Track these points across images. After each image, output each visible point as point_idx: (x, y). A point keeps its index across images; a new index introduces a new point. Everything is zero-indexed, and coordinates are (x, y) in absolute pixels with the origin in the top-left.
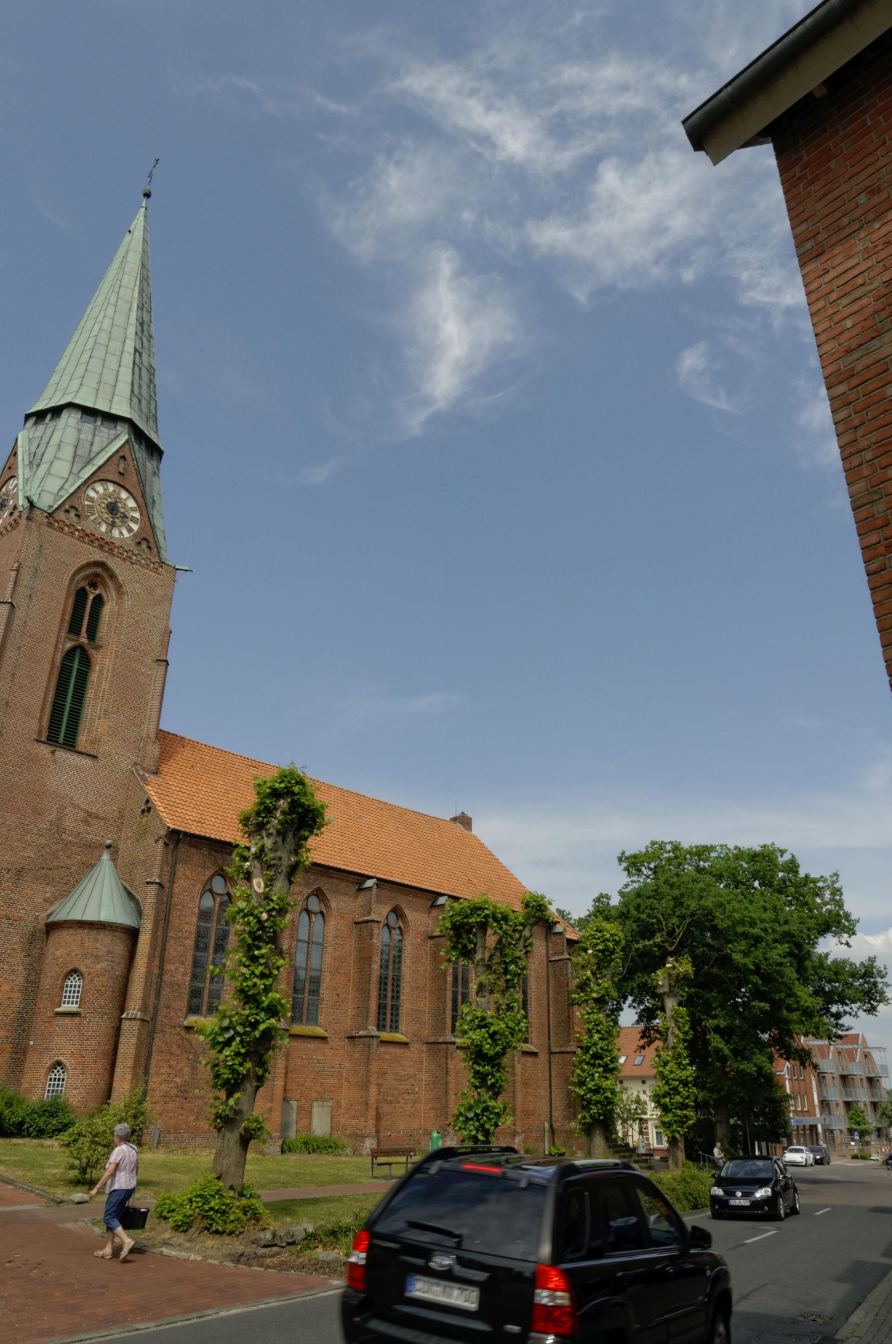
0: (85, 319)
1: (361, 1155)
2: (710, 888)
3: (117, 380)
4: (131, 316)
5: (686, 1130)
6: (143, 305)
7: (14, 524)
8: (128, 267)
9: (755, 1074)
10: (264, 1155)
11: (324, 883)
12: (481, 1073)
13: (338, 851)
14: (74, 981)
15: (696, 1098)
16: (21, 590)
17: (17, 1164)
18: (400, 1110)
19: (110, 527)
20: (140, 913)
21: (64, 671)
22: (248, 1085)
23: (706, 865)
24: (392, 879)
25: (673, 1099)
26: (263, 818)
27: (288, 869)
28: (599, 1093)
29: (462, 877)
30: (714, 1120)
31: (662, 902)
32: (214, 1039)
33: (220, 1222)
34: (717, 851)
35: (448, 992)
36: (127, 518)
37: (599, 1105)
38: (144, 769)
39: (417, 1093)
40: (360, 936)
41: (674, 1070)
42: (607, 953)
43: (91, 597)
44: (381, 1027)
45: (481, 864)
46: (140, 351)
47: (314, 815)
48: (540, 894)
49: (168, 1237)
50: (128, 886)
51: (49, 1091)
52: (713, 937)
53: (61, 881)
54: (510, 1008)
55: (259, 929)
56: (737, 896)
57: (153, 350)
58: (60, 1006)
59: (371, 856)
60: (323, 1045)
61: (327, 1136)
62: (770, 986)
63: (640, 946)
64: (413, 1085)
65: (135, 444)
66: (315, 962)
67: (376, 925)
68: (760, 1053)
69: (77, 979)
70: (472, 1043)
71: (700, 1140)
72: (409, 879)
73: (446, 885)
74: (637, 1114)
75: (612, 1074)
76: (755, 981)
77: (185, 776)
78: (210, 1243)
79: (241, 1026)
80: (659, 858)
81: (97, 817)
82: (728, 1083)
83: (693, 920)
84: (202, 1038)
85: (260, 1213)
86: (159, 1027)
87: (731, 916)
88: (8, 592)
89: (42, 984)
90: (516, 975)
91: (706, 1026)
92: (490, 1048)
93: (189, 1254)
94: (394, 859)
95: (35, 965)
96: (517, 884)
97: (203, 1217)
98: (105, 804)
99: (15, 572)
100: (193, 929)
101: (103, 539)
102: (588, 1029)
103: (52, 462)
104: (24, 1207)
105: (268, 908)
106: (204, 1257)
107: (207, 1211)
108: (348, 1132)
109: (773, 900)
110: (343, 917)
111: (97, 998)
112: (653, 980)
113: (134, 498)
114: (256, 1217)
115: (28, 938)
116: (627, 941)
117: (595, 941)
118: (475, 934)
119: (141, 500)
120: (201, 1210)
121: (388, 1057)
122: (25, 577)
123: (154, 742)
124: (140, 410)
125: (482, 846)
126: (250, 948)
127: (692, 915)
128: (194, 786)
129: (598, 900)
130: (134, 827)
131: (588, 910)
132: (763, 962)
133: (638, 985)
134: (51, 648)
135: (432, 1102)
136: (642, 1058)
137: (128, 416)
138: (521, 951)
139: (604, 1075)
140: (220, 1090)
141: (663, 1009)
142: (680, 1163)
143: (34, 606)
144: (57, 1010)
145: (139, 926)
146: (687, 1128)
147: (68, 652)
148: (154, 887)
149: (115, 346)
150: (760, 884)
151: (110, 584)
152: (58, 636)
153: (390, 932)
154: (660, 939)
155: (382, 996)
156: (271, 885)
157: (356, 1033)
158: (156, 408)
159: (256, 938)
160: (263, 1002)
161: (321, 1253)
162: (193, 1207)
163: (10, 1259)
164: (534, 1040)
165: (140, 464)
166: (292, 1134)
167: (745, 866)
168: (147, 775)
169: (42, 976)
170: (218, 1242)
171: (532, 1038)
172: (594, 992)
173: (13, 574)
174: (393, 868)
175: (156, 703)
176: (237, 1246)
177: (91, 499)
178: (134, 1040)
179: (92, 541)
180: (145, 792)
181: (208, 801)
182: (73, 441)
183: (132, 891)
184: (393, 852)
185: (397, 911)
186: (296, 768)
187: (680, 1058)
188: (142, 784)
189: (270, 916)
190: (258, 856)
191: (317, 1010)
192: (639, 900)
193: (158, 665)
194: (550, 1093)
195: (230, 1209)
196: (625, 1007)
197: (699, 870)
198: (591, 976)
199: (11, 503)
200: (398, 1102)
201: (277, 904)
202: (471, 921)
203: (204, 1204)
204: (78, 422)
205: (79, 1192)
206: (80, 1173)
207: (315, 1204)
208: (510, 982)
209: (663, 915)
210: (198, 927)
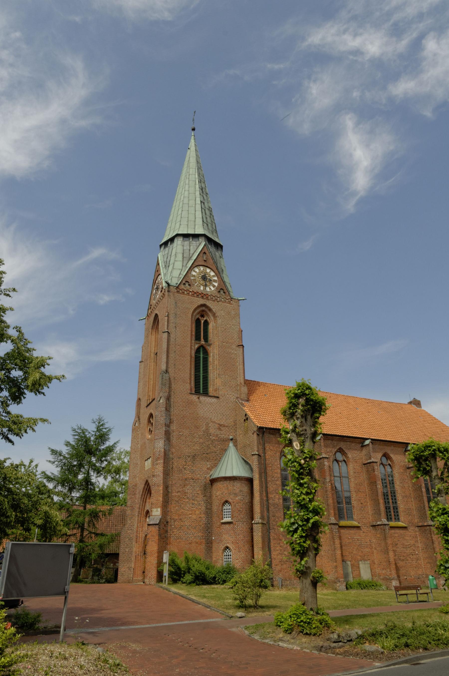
1: (391, 590)
3: (195, 218)
6: (201, 180)
8: (191, 165)
11: (342, 445)
13: (347, 427)
14: (227, 507)
16: (171, 325)
17: (212, 598)
18: (409, 564)
19: (205, 287)
20: (252, 469)
21: (197, 359)
22: (310, 553)
24: (380, 438)
26: (293, 410)
27: (311, 435)
29: (420, 433)
32: (288, 529)
33: (308, 628)
36: (212, 281)
38: (242, 400)
39: (417, 554)
40: (368, 471)
43: (202, 322)
45: (430, 425)
46: (203, 201)
47: (320, 405)
49: (282, 636)
51: (225, 561)
53: (213, 459)
55: (301, 469)
57: (209, 199)
59: (365, 428)
60: (358, 531)
61: (370, 580)
64: (414, 550)
67: (375, 464)
69: (228, 505)
70: (440, 523)
73: (412, 438)
77: (262, 400)
78: (304, 640)
79: (301, 522)
81: (224, 426)
85: (329, 624)
86: (271, 526)
89: (213, 509)
95: (209, 500)
97: (299, 625)
100: (279, 475)
101: (203, 293)
103: (174, 263)
104: (214, 620)
105: (304, 457)
106: (301, 648)
107: (300, 622)
108: (381, 577)
111: (239, 514)
113: (213, 271)
114: (328, 626)
115: (203, 488)
118: (429, 461)
120: (297, 622)
121: (396, 535)
126: (298, 479)
130: (242, 429)
134: (189, 349)
135: (427, 559)
137: (203, 233)
140: (296, 556)
143: (178, 331)
144: (222, 521)
145: (252, 477)
147: (197, 350)
148: (256, 457)
149: (192, 203)
151: (210, 314)
152: (191, 343)
153: (384, 467)
155: (386, 502)
156: (304, 445)
157: (376, 523)
158: (215, 226)
160: (310, 508)
161: (367, 646)
162: (292, 620)
163: (203, 648)
166: (351, 579)
168: (243, 402)
173: (166, 318)
174: (379, 433)
175: (241, 367)
176: (319, 642)
177: (194, 276)
178: (260, 534)
180: (244, 411)
182: (182, 251)
183: (247, 460)
184: (377, 424)
185: (386, 455)
186: (305, 381)
188: (242, 407)
189: (306, 461)
190: (294, 431)
191: (352, 512)
193: (239, 348)
195: (312, 621)
199: (160, 286)
200: (408, 560)
201: (308, 454)
202: (425, 454)
203: (298, 618)
205: (240, 612)
207: (363, 618)
210: (282, 474)
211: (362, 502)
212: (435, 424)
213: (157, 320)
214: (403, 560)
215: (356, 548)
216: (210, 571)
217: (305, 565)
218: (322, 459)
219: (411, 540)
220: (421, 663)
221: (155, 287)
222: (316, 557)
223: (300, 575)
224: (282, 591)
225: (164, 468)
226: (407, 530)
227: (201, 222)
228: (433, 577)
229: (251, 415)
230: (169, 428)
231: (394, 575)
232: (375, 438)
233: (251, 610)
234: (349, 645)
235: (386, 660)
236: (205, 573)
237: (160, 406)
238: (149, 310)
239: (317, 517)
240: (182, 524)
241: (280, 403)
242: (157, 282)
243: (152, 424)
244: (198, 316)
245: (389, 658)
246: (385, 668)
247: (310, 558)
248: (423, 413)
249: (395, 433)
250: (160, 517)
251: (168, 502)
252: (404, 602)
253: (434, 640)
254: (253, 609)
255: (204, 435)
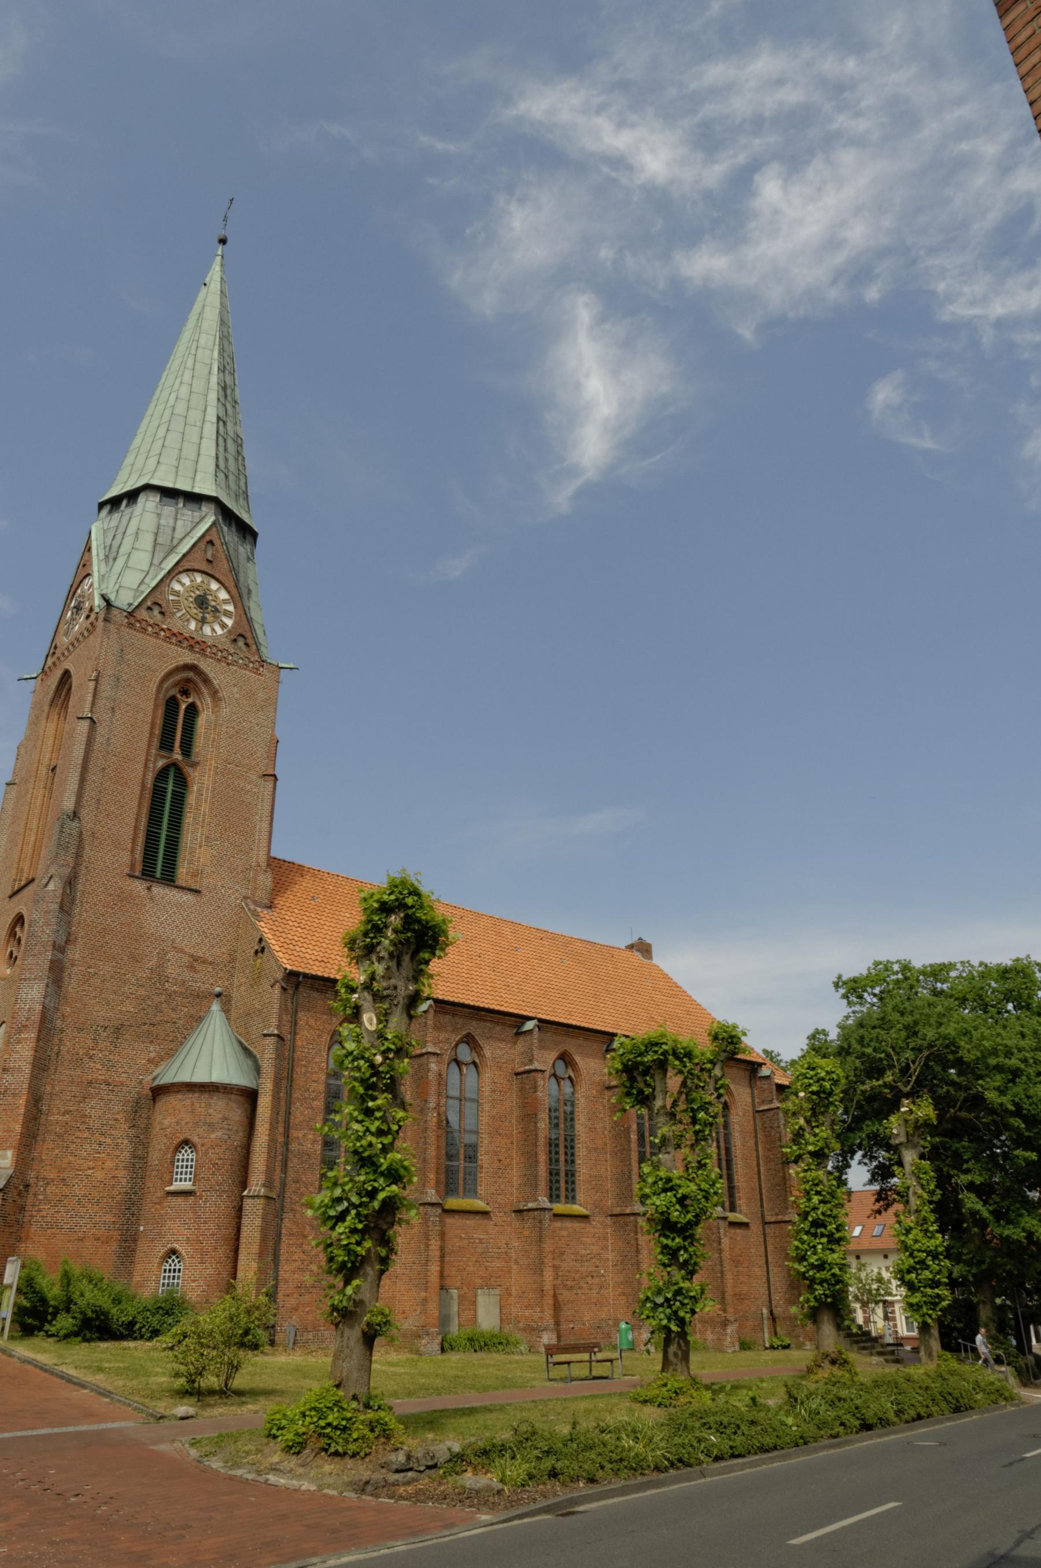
0: (159, 389)
1: (538, 1352)
2: (952, 1012)
3: (199, 455)
4: (211, 380)
5: (939, 1313)
6: (224, 367)
7: (90, 628)
8: (205, 325)
9: (1025, 1241)
10: (421, 1355)
11: (475, 1028)
12: (670, 1248)
13: (490, 989)
14: (186, 1155)
15: (951, 1273)
16: (101, 703)
17: (119, 1372)
18: (583, 1297)
19: (200, 624)
20: (258, 1070)
21: (158, 794)
22: (369, 1269)
23: (945, 986)
24: (557, 1019)
25: (920, 1274)
26: (372, 938)
28: (824, 1269)
30: (975, 1300)
31: (891, 1032)
32: (325, 1213)
33: (341, 1441)
34: (957, 970)
35: (633, 1153)
37: (824, 1284)
38: (255, 903)
39: (603, 1276)
40: (522, 1090)
41: (918, 1238)
42: (822, 1095)
43: (183, 706)
44: (554, 1197)
45: (665, 998)
46: (224, 419)
48: (730, 1023)
50: (243, 1041)
52: (959, 1074)
53: (167, 1038)
54: (701, 1165)
55: (372, 1075)
56: (986, 1020)
57: (240, 417)
58: (172, 1184)
61: (497, 1330)
62: (1036, 1130)
63: (867, 1087)
64: (597, 1267)
65: (224, 527)
66: (469, 1123)
67: (540, 1075)
68: (1029, 1215)
69: (189, 1151)
71: (960, 1325)
72: (578, 1019)
73: (623, 1024)
74: (880, 1295)
75: (839, 1245)
76: (1016, 1124)
78: (328, 1468)
80: (885, 981)
81: (204, 962)
82: (990, 1253)
83: (932, 1054)
84: (310, 1213)
85: (391, 1429)
86: (287, 1206)
87: (980, 1045)
88: (87, 706)
90: (706, 1124)
91: (957, 1184)
92: (680, 1216)
93: (301, 1483)
94: (559, 995)
95: (142, 1137)
96: (700, 1011)
97: (320, 1435)
98: (213, 946)
99: (94, 682)
100: (322, 1088)
101: (193, 638)
102: (805, 1190)
103: (130, 553)
105: (382, 1048)
107: (323, 1428)
108: (521, 1325)
109: (1032, 1024)
110: (500, 1067)
112: (886, 1128)
114: (387, 1435)
115: (132, 1106)
116: (850, 1082)
117: (806, 1081)
118: (652, 1077)
119: (234, 591)
120: (317, 1427)
121: (565, 1233)
122: (106, 686)
123: (265, 871)
124: (228, 487)
125: (665, 976)
126: (363, 1099)
127: (930, 1046)
128: (316, 920)
129: (813, 1037)
130: (248, 971)
131: (802, 1050)
132: (1025, 1100)
133: (868, 1136)
134: (140, 767)
135: (622, 1286)
136: (882, 1227)
137: (214, 494)
138: (712, 1094)
139: (830, 1247)
140: (336, 1276)
141: (900, 1163)
142: (935, 1354)
143: (117, 720)
144: (167, 1188)
145: (258, 1086)
146: (941, 1310)
147: (160, 772)
149: (195, 416)
150: (1014, 1007)
151: (204, 690)
153: (559, 1083)
154: (891, 1078)
155: (553, 1161)
156: (387, 1021)
159: (370, 1087)
160: (382, 1165)
161: (470, 1479)
162: (306, 1423)
164: (744, 1208)
165: (231, 552)
166: (454, 1329)
167: (993, 984)
168: (259, 910)
169: (150, 1149)
170: (338, 1466)
171: (740, 1206)
172: (810, 1144)
173: (92, 685)
174: (557, 1007)
175: (265, 825)
176: (362, 1471)
177: (177, 593)
178: (258, 1222)
179: (180, 641)
180: (258, 930)
181: (332, 937)
182: (153, 528)
183: (249, 1047)
184: (556, 988)
185: (565, 1058)
187: (926, 1223)
190: (367, 987)
191: (475, 1180)
192: (862, 1031)
193: (265, 781)
194: (768, 1273)
195: (353, 1424)
196: (854, 1163)
197: (936, 993)
198: (805, 1125)
200: (581, 1288)
201: (394, 1043)
202: (646, 1060)
203: (320, 1418)
204: (157, 507)
205: (186, 1404)
206: (188, 1382)
207: (469, 1415)
208: (701, 1134)
209: (893, 1048)
210: (328, 1085)
211: (501, 1158)
212: (674, 996)
213: (67, 686)
214: (572, 1288)
215: (474, 1259)
216: (123, 1308)
217: (353, 1296)
218: (426, 1057)
219: (593, 1244)
220: (577, 1512)
221: (72, 605)
222: (380, 1279)
223: (339, 1319)
224: (294, 1355)
225: (36, 1051)
226: (589, 1222)
227: (212, 467)
228: (629, 1326)
229: (273, 942)
230: (63, 953)
231: (549, 1320)
232: (548, 1018)
233: (211, 1400)
234: (430, 1477)
235: (506, 1508)
236: (109, 1313)
237: (47, 899)
238: (49, 658)
239: (394, 1188)
240: (66, 1191)
241: (347, 920)
242: (79, 591)
243: (19, 940)
244: (172, 692)
245: (511, 1504)
246: (501, 1526)
247: (366, 1280)
248: (654, 971)
249: (590, 1009)
250: (10, 1172)
251: (34, 1137)
252: (562, 1380)
253: (610, 1462)
254: (217, 1397)
255: (150, 979)
